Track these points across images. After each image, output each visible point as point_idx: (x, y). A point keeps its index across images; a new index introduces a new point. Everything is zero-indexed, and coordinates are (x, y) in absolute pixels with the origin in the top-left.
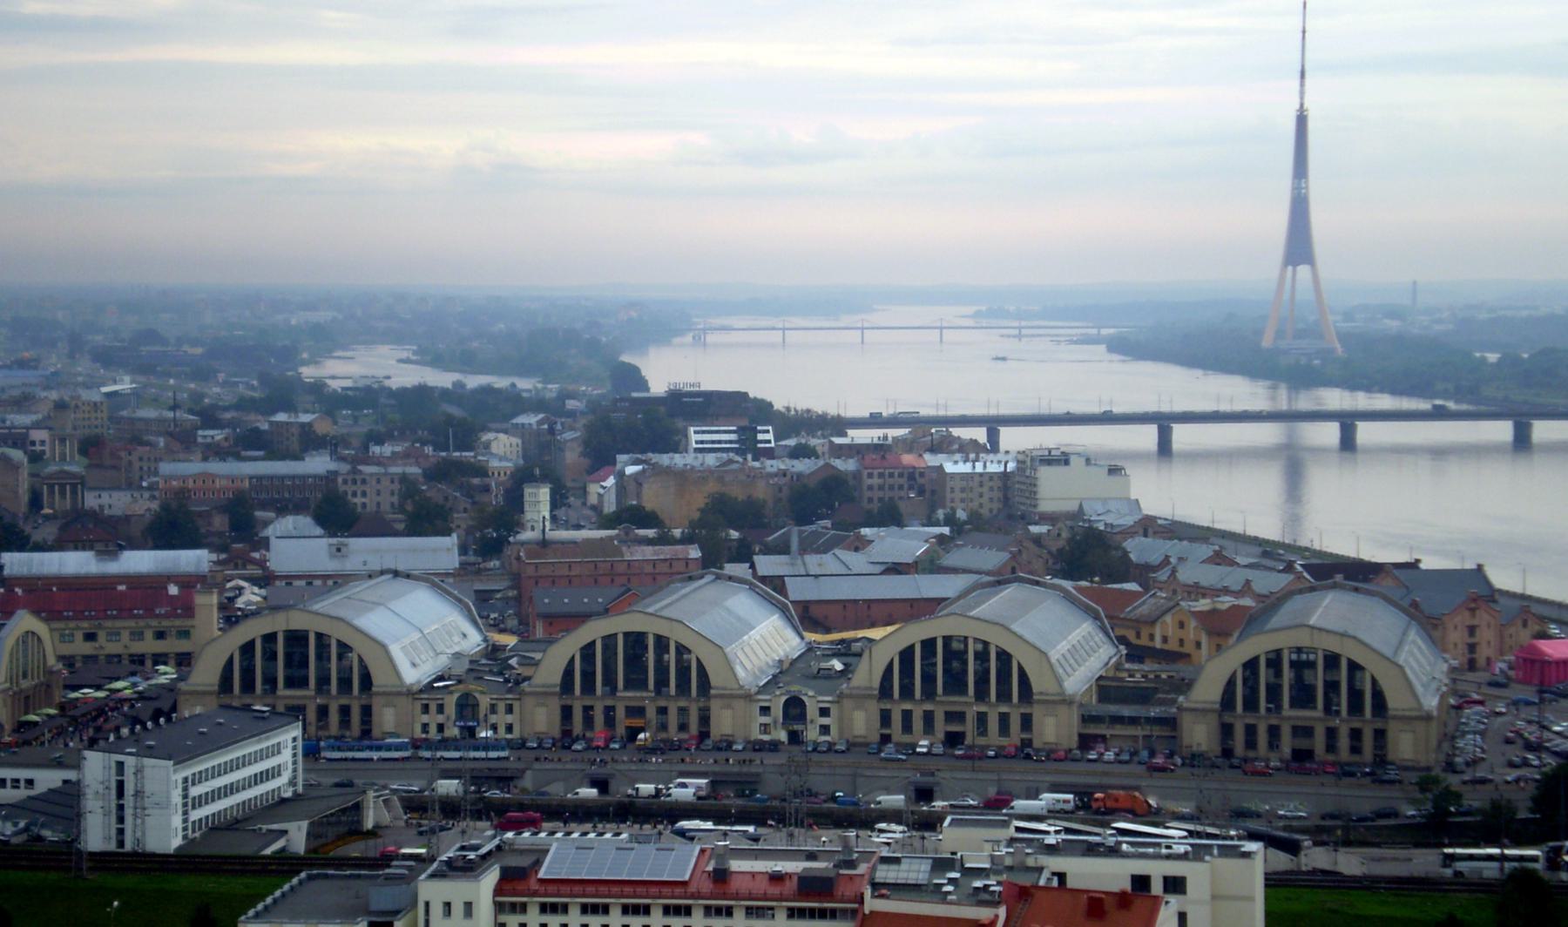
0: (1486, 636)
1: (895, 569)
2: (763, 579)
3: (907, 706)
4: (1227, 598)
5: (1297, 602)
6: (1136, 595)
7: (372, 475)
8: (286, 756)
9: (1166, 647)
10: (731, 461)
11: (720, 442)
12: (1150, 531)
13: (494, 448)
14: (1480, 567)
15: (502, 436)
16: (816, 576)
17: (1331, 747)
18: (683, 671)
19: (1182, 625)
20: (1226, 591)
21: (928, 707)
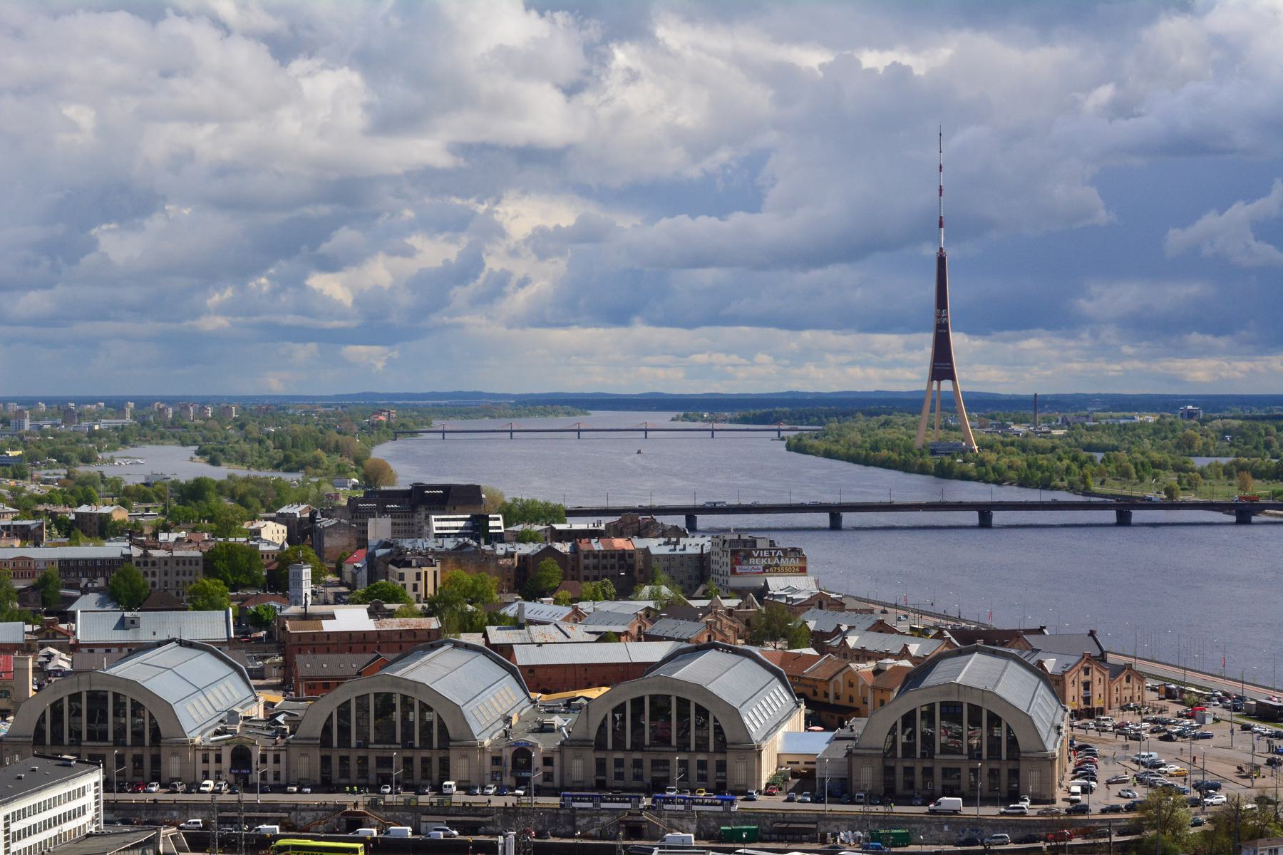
1: (604, 638)
2: (495, 647)
4: (889, 661)
5: (943, 666)
6: (811, 659)
7: (160, 558)
8: (89, 799)
9: (837, 702)
10: (466, 545)
11: (446, 528)
12: (825, 603)
13: (264, 535)
15: (270, 523)
16: (540, 644)
18: (426, 727)
20: (888, 655)
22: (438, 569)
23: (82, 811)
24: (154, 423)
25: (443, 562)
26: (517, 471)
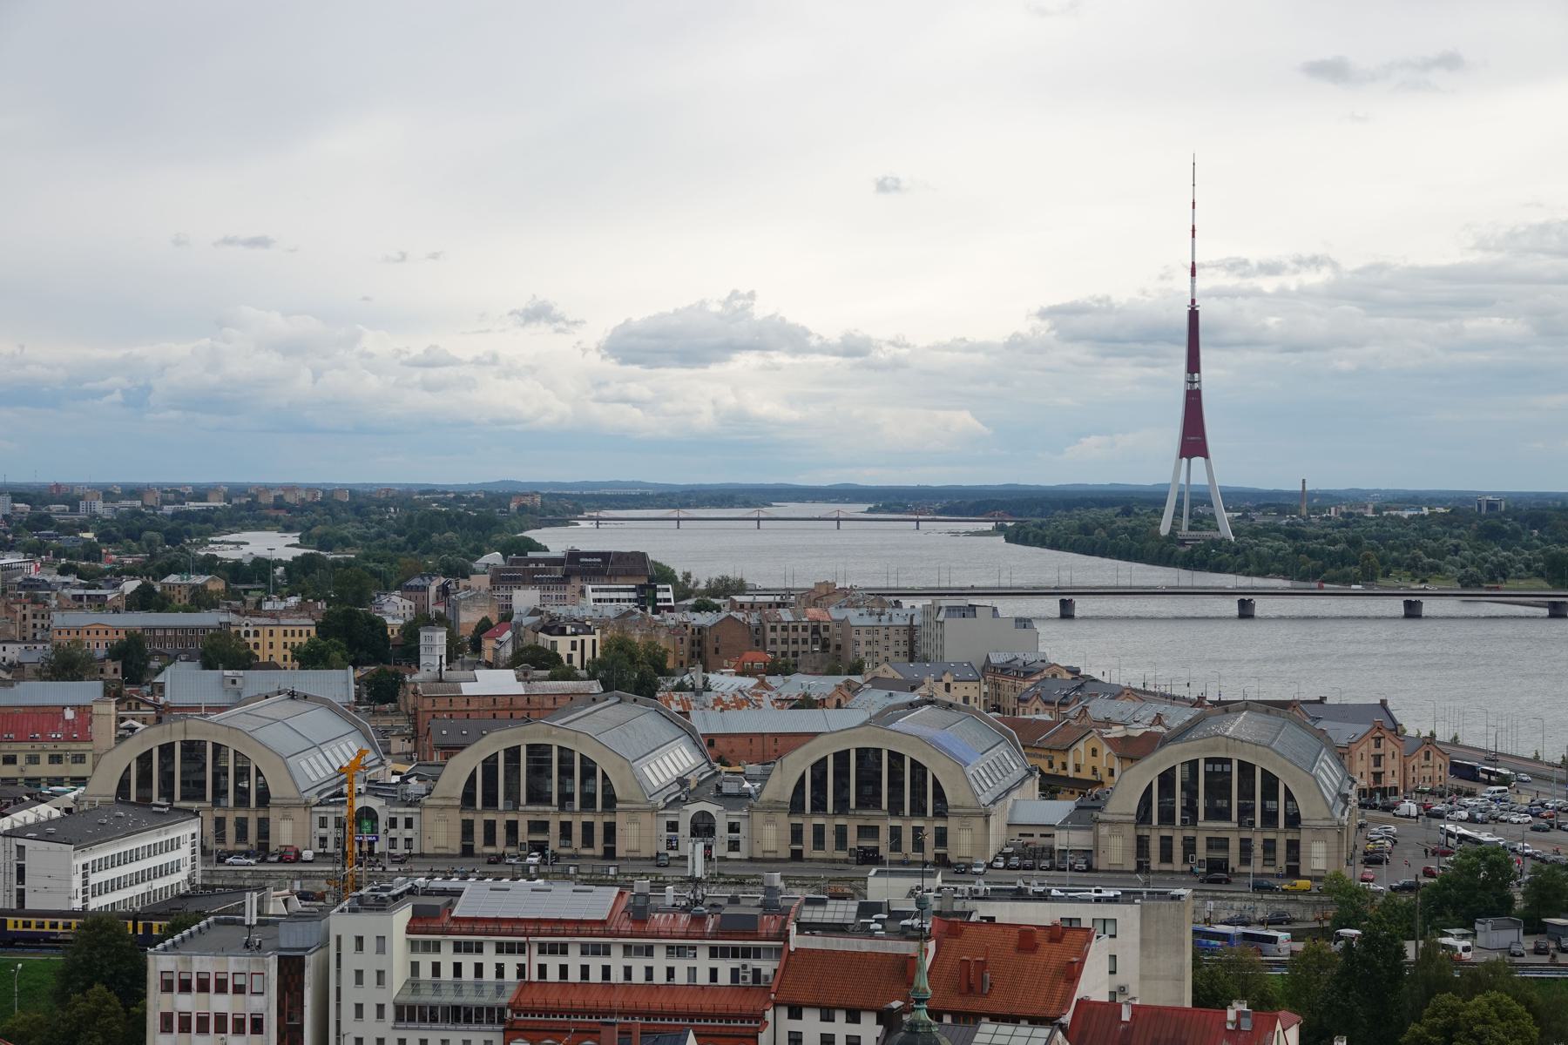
0: (1391, 765)
3: (819, 821)
8: (184, 852)
9: (1078, 775)
10: (631, 613)
14: (1383, 703)
17: (1245, 860)
19: (1094, 752)
21: (841, 821)
22: (597, 637)
23: (174, 868)
24: (252, 509)
25: (603, 629)
26: (693, 550)
